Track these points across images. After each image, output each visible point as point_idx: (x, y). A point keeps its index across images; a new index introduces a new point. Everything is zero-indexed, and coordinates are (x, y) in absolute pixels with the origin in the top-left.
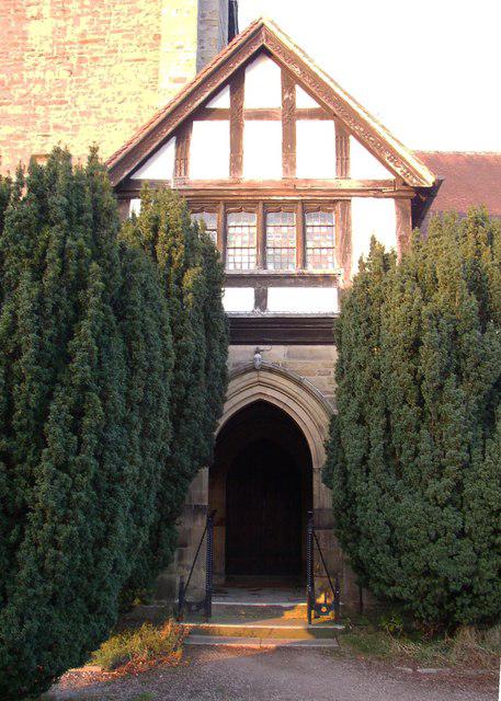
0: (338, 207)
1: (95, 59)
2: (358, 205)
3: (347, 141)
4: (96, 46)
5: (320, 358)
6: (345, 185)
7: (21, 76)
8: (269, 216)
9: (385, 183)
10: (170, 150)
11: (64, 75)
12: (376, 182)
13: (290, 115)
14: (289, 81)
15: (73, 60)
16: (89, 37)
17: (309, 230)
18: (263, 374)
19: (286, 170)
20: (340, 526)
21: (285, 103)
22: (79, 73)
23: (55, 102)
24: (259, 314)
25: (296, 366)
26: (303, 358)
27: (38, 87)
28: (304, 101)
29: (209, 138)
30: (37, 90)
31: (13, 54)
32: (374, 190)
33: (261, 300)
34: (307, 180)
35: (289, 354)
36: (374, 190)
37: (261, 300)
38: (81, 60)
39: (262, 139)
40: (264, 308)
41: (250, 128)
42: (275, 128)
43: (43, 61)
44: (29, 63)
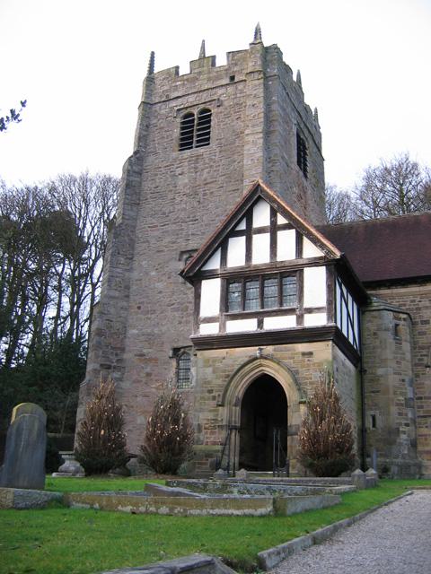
0: (298, 274)
1: (212, 193)
2: (307, 271)
3: (302, 239)
4: (212, 185)
5: (289, 350)
6: (301, 262)
7: (174, 208)
8: (248, 284)
9: (320, 258)
10: (218, 256)
11: (196, 204)
12: (315, 258)
13: (274, 229)
14: (273, 214)
15: (201, 195)
16: (208, 181)
17: (266, 289)
18: (262, 360)
19: (271, 258)
20: (60, 360)
21: (272, 222)
22: (204, 202)
23: (192, 221)
24: (259, 331)
25: (279, 355)
26: (281, 351)
27: (183, 213)
28: (281, 220)
29: (236, 247)
30: (182, 215)
31: (170, 196)
32: (315, 263)
33: (260, 324)
34: (282, 262)
35: (275, 350)
36: (315, 263)
37: (260, 324)
38: (205, 195)
39: (261, 242)
40: (262, 328)
41: (256, 238)
42: (267, 236)
43: (185, 198)
44: (178, 199)
